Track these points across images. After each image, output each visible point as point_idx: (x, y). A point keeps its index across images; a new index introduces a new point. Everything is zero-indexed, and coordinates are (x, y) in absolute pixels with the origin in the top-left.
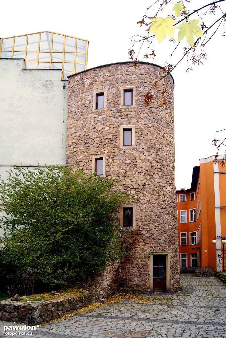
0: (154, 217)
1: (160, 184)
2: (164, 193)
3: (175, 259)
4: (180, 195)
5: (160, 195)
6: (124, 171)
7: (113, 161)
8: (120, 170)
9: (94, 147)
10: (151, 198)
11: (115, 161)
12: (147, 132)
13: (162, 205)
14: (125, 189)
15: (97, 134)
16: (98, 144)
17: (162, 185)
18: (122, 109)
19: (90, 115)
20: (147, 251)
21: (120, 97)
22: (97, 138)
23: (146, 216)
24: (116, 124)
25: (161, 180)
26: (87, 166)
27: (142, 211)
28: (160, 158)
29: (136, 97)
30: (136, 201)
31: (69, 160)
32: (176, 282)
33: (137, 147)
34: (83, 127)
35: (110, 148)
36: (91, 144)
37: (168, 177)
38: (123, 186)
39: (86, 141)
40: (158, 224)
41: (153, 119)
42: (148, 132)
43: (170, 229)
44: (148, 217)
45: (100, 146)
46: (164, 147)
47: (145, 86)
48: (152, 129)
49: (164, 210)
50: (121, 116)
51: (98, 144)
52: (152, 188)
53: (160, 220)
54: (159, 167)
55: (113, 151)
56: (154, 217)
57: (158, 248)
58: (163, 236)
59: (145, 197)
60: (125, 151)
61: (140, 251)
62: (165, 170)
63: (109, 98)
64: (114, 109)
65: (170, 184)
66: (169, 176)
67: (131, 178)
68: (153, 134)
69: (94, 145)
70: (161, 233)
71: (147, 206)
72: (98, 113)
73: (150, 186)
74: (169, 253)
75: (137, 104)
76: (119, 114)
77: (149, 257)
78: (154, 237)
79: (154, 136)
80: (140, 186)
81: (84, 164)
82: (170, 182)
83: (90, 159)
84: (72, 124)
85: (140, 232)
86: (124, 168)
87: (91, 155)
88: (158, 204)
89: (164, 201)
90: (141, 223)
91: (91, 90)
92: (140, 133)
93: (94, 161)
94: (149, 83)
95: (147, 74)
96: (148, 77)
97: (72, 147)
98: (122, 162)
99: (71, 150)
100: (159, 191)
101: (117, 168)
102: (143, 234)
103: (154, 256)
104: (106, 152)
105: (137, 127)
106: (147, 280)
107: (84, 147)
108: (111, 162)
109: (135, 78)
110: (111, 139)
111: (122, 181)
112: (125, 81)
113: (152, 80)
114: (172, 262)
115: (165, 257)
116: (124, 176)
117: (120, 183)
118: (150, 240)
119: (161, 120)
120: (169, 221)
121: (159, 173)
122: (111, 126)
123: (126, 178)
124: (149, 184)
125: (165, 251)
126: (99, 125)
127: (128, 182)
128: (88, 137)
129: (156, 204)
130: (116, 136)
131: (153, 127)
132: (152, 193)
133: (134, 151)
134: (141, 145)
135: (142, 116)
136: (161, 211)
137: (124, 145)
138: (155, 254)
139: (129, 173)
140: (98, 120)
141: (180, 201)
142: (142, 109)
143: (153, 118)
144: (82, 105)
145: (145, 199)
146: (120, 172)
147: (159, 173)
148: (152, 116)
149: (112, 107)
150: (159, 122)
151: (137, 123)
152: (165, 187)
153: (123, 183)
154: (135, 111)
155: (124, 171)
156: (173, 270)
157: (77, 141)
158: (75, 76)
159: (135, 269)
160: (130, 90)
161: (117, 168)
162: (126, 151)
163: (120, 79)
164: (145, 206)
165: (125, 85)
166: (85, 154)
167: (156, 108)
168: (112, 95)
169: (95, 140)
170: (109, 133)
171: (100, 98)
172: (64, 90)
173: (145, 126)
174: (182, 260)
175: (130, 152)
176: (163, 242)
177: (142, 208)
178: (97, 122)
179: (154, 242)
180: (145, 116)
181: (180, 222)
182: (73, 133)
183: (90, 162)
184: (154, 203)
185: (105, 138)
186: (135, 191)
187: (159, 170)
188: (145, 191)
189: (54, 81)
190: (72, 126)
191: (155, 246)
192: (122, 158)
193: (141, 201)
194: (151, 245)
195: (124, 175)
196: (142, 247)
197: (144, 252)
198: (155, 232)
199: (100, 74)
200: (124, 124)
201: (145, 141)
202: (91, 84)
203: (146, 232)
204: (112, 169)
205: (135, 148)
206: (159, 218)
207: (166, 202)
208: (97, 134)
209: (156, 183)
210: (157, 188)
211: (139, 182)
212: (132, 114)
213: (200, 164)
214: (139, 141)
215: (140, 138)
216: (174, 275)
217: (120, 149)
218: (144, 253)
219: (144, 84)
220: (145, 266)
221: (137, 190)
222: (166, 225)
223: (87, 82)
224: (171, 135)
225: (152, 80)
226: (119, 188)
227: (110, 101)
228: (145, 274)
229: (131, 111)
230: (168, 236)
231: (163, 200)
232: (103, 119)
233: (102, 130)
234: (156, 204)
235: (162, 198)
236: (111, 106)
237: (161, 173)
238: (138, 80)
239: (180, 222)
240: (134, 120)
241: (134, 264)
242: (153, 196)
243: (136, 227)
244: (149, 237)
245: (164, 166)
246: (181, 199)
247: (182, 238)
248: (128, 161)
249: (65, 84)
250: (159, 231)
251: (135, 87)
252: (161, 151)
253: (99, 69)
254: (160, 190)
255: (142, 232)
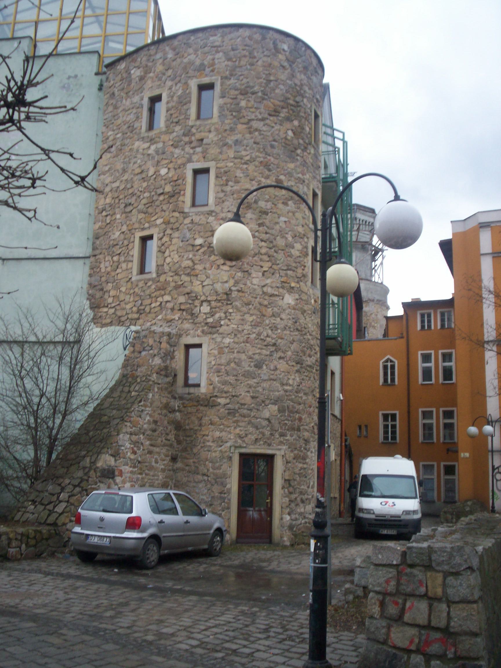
0: (246, 366)
1: (265, 289)
2: (276, 309)
3: (301, 465)
4: (439, 311)
5: (264, 316)
6: (190, 263)
7: (170, 243)
8: (182, 261)
9: (140, 212)
10: (242, 322)
11: (174, 241)
12: (239, 173)
13: (268, 336)
14: (190, 302)
15: (145, 185)
16: (147, 206)
17: (269, 290)
18: (192, 127)
19: (137, 144)
20: (228, 444)
21: (190, 102)
22: (145, 192)
23: (228, 364)
24: (179, 162)
25: (268, 281)
26: (126, 255)
27: (221, 351)
28: (268, 231)
29: (221, 100)
30: (210, 330)
31: (98, 242)
32: (299, 522)
33: (218, 209)
34: (124, 171)
35: (167, 213)
36: (134, 206)
37: (289, 272)
38: (186, 295)
39: (127, 201)
40: (255, 380)
41: (254, 145)
42: (242, 175)
43: (287, 394)
44: (233, 365)
45: (150, 210)
46: (280, 206)
47: (240, 73)
48: (251, 167)
49: (273, 349)
50: (191, 142)
51: (147, 206)
52: (245, 300)
53: (259, 372)
54: (263, 251)
55: (172, 220)
56: (246, 366)
57: (253, 438)
58: (266, 410)
59: (229, 319)
60: (194, 218)
61: (211, 444)
62: (280, 256)
63: (170, 105)
64: (177, 128)
65: (293, 288)
66: (290, 270)
67: (203, 277)
68: (252, 178)
69: (139, 207)
70: (263, 402)
71: (232, 340)
72: (149, 139)
73: (241, 294)
74: (280, 450)
75: (222, 116)
76: (187, 139)
77: (230, 458)
78: (245, 411)
79: (254, 182)
80: (219, 295)
81: (121, 250)
82: (293, 285)
83: (132, 240)
84: (106, 165)
85: (214, 401)
86: (191, 256)
87: (133, 231)
88: (259, 334)
89: (274, 328)
90: (217, 379)
91: (141, 90)
92: (224, 178)
93: (137, 242)
94: (249, 67)
95: (244, 48)
96: (247, 54)
97: (104, 213)
98: (188, 243)
99: (102, 222)
100: (260, 304)
101: (176, 258)
102: (220, 404)
103: (241, 455)
104: (159, 222)
105: (219, 165)
106: (223, 513)
107: (122, 213)
108: (166, 244)
109: (220, 60)
110: (170, 194)
111: (186, 284)
112: (201, 68)
113: (255, 60)
114: (287, 473)
115: (270, 459)
116: (188, 275)
117: (181, 289)
118: (236, 418)
119: (272, 147)
120: (283, 374)
121: (262, 263)
122: (171, 166)
123: (194, 279)
124: (239, 291)
125: (269, 445)
126: (149, 163)
127: (197, 287)
128: (130, 191)
129: (254, 335)
130: (179, 188)
131: (253, 163)
132: (244, 309)
133: (211, 219)
134: (225, 203)
135: (230, 141)
136: (264, 352)
137: (193, 205)
138: (243, 451)
139: (199, 267)
140: (149, 155)
141: (439, 327)
142: (232, 125)
143: (255, 143)
144: (125, 124)
145: (228, 325)
146: (183, 266)
147: (262, 263)
148: (252, 138)
149: (174, 124)
150: (269, 150)
151: (220, 157)
152: (276, 295)
153: (187, 290)
154: (217, 130)
155: (190, 263)
156: (291, 493)
157: (113, 202)
158: (117, 64)
159: (201, 485)
160: (210, 87)
161: (176, 256)
162: (196, 219)
163: (191, 63)
164: (227, 341)
165: (201, 75)
166: (124, 228)
167: (263, 119)
168: (175, 98)
169: (142, 197)
170: (166, 181)
171: (204, 94)
172: (101, 94)
173: (236, 161)
174: (447, 482)
175: (203, 219)
176: (265, 423)
177: (222, 345)
178: (146, 158)
179: (243, 424)
180: (237, 141)
181: (420, 383)
182: (107, 185)
183: (130, 247)
184: (249, 334)
185: (160, 191)
186: (209, 308)
187: (265, 258)
188: (230, 306)
189: (82, 76)
190: (107, 168)
191: (247, 432)
192: (188, 235)
193: (221, 330)
194: (237, 431)
195: (189, 271)
196: (217, 434)
197: (221, 446)
198: (248, 400)
199: (158, 56)
200: (195, 160)
201: (235, 196)
202: (142, 78)
203: (228, 401)
204: (168, 260)
205: (212, 211)
206: (258, 366)
207: (279, 331)
208: (145, 185)
209: (256, 287)
210: (258, 299)
211: (218, 287)
212: (212, 137)
213: (454, 234)
214: (221, 195)
215: (225, 188)
216: (293, 505)
217: (185, 215)
218: (220, 449)
219: (238, 69)
220: (221, 480)
221: (213, 304)
222: (277, 384)
223: (136, 73)
224: (300, 175)
225: (255, 60)
226: (179, 302)
227: (172, 112)
228: (221, 497)
229: (210, 131)
230: (281, 410)
231: (270, 325)
232: (157, 152)
233: (155, 176)
234: (253, 336)
235: (267, 322)
236: (172, 122)
237: (269, 264)
238: (226, 62)
239: (420, 383)
240: (213, 151)
241: (198, 474)
242: (247, 316)
243: (208, 388)
244: (232, 413)
245: (276, 249)
246: (443, 320)
247: (424, 425)
248: (199, 241)
249: (101, 81)
250: (257, 397)
251: (220, 78)
252: (270, 214)
253: (157, 45)
254: (266, 303)
255: (219, 400)
